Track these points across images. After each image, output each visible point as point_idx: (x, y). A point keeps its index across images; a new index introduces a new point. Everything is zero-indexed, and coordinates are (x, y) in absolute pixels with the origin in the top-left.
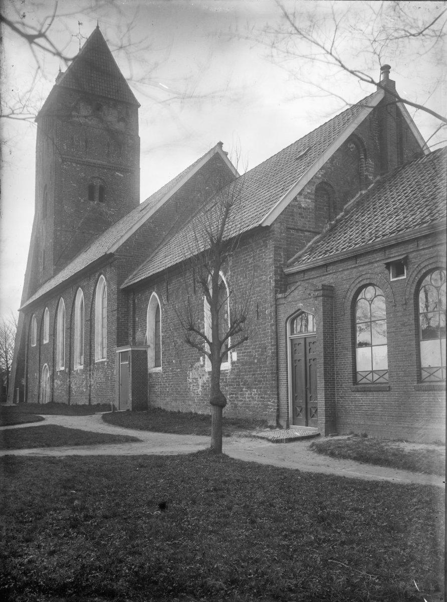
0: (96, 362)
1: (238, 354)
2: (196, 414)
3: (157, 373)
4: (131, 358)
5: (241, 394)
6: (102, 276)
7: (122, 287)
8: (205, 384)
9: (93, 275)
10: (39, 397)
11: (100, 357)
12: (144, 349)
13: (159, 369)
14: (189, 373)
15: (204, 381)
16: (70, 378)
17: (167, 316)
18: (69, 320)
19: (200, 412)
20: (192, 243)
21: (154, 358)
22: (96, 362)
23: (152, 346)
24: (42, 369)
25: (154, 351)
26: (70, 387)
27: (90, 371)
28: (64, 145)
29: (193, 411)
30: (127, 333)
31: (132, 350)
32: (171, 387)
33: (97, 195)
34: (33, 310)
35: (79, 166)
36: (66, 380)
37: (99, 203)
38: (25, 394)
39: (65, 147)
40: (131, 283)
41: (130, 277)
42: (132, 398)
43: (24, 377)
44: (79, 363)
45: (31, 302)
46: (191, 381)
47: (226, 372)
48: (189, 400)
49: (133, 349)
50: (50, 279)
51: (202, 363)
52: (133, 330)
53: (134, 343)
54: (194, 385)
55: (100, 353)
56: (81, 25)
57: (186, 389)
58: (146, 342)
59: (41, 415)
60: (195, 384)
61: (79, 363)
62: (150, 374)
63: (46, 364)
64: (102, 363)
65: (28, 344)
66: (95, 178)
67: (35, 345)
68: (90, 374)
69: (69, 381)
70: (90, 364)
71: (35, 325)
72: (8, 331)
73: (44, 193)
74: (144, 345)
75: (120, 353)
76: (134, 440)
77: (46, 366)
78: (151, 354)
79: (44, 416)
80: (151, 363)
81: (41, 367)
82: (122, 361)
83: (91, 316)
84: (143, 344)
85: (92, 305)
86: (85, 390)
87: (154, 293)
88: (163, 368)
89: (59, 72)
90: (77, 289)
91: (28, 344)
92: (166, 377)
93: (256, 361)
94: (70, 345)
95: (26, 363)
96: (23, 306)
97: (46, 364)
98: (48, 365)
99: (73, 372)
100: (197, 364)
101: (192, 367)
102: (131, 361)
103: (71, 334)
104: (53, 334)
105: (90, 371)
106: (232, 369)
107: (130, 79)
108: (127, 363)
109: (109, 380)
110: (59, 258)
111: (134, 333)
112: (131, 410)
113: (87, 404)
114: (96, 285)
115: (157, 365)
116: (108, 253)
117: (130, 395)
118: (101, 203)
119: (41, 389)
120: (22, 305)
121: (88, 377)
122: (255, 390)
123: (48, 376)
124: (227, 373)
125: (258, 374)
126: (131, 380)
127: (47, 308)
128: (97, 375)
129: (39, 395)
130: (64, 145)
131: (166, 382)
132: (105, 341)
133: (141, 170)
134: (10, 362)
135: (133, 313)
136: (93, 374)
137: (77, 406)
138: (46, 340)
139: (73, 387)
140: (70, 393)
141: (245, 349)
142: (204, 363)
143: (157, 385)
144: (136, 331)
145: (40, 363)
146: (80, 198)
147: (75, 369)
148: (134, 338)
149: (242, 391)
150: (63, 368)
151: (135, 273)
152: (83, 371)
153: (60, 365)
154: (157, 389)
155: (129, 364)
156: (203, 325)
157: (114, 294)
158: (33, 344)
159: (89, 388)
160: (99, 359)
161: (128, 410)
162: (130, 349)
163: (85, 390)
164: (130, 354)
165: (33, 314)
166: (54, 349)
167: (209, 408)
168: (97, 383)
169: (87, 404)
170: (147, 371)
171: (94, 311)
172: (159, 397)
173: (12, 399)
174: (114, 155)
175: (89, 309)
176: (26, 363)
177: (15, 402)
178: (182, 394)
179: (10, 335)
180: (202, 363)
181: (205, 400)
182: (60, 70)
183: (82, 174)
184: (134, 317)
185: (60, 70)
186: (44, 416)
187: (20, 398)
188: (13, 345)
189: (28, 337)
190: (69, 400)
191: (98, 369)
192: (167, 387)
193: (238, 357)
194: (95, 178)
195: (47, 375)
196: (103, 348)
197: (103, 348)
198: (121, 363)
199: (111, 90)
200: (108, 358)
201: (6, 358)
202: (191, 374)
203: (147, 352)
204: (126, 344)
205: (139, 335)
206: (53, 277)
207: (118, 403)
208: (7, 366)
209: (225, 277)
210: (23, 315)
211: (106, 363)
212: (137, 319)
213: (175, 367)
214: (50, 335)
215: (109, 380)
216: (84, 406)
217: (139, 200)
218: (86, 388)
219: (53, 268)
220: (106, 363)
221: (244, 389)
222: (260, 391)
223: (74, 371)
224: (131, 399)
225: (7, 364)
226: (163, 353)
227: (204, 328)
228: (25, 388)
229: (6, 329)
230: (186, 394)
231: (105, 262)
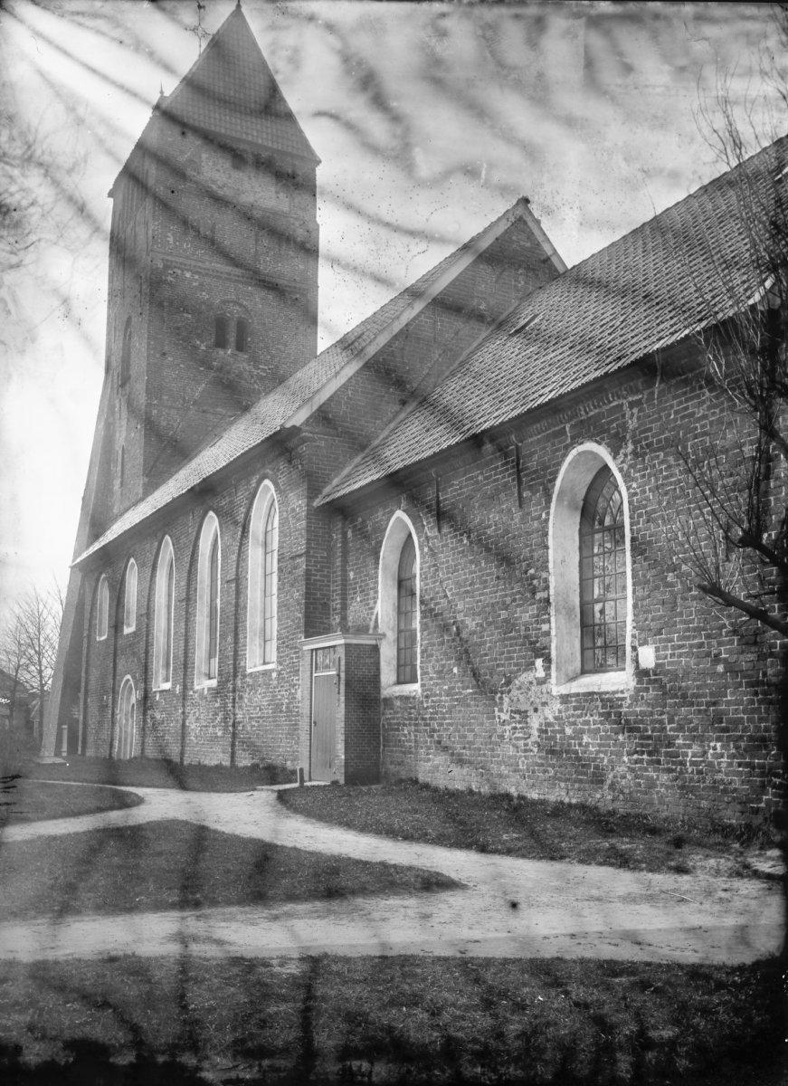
0: (249, 671)
1: (657, 650)
2: (521, 798)
3: (405, 699)
4: (343, 663)
5: (667, 754)
6: (267, 482)
7: (317, 503)
8: (548, 724)
9: (243, 482)
10: (111, 746)
11: (259, 660)
12: (374, 642)
13: (414, 689)
14: (501, 698)
15: (546, 719)
16: (184, 706)
17: (435, 565)
18: (183, 583)
19: (534, 795)
20: (393, 456)
21: (395, 662)
22: (249, 671)
23: (391, 636)
24: (119, 686)
25: (396, 647)
26: (184, 725)
27: (234, 691)
28: (169, 234)
29: (513, 791)
30: (326, 606)
31: (347, 646)
32: (447, 730)
33: (232, 338)
34: (104, 566)
35: (197, 277)
36: (176, 710)
37: (237, 353)
38: (80, 738)
39: (171, 240)
40: (338, 495)
41: (335, 482)
42: (345, 753)
43: (78, 704)
44: (205, 674)
45: (96, 549)
46: (504, 717)
47: (620, 695)
48: (499, 763)
49: (349, 641)
50: (135, 504)
51: (541, 673)
52: (342, 599)
53: (345, 630)
54: (515, 728)
55: (258, 651)
56: (202, 10)
57: (490, 737)
58: (376, 626)
59: (123, 788)
60: (518, 726)
61: (205, 674)
62: (386, 700)
63: (129, 677)
64: (266, 673)
65: (89, 636)
66: (229, 302)
67: (103, 638)
68: (234, 699)
69: (183, 713)
70: (235, 676)
71: (104, 594)
72: (45, 612)
73: (125, 333)
74: (371, 631)
75: (312, 650)
76: (433, 884)
77: (128, 680)
78: (388, 653)
79: (140, 791)
80: (387, 675)
81: (117, 688)
82: (316, 669)
83: (237, 571)
84: (368, 630)
85: (240, 547)
86: (220, 734)
87: (399, 514)
88: (423, 685)
89: (159, 95)
90: (206, 513)
91: (89, 636)
92: (433, 707)
93: (720, 668)
94: (186, 635)
95: (83, 675)
96: (78, 560)
97: (129, 677)
98: (134, 677)
99: (191, 693)
100: (525, 677)
101: (508, 682)
102: (343, 668)
103: (187, 612)
104: (147, 614)
105: (234, 691)
106: (637, 690)
107: (299, 113)
108: (334, 673)
109: (281, 711)
110: (155, 462)
111: (344, 607)
112: (342, 782)
113: (227, 763)
114: (251, 504)
115: (586, 668)
116: (288, 425)
117: (340, 747)
118: (240, 354)
119: (117, 729)
120: (75, 557)
121: (230, 705)
122: (719, 745)
123: (133, 700)
124: (623, 699)
125: (728, 703)
126: (343, 711)
127: (132, 560)
128: (250, 700)
129: (112, 740)
130: (169, 234)
131: (431, 719)
132: (274, 626)
133: (320, 290)
134: (48, 672)
135: (342, 561)
136: (241, 698)
137: (201, 768)
138: (129, 625)
139: (192, 725)
140: (183, 738)
141: (680, 639)
142: (548, 676)
143: (404, 725)
144: (349, 602)
145: (114, 676)
146: (198, 342)
147: (197, 687)
148: (344, 618)
149: (670, 745)
150: (167, 686)
151: (346, 472)
152: (217, 693)
153: (160, 679)
154: (405, 736)
155: (339, 675)
156: (546, 580)
157: (298, 520)
158: (100, 636)
159: (230, 728)
160: (255, 666)
161: (335, 783)
162: (342, 641)
163: (220, 734)
164: (341, 653)
165: (101, 573)
166: (148, 645)
167: (563, 785)
168: (250, 718)
169: (227, 763)
170: (379, 693)
171: (245, 560)
172: (411, 753)
173: (53, 749)
174: (268, 259)
175: (234, 557)
176: (83, 675)
177: (58, 754)
178: (480, 749)
179: (50, 619)
180: (541, 673)
181: (550, 765)
182: (162, 92)
183: (204, 293)
184: (345, 572)
185: (162, 92)
186: (140, 791)
187: (69, 743)
188: (55, 639)
189: (90, 621)
190: (182, 753)
191: (252, 687)
192: (434, 731)
193: (657, 658)
194: (229, 302)
195: (128, 699)
196: (265, 641)
197: (265, 641)
198: (315, 675)
199: (265, 130)
200: (280, 663)
201: (40, 665)
202: (506, 700)
203: (379, 649)
204: (326, 630)
205: (355, 610)
206: (142, 499)
207: (308, 765)
208: (41, 681)
209: (614, 458)
210: (79, 575)
211: (274, 675)
212: (352, 575)
213: (459, 684)
214: (139, 617)
215: (281, 711)
216: (219, 768)
217: (316, 348)
218: (225, 728)
219: (141, 481)
220: (274, 675)
221: (680, 741)
222: (737, 748)
223: (194, 692)
224: (343, 757)
225: (41, 677)
226: (422, 652)
227: (547, 588)
228: (81, 726)
229: (41, 607)
230: (493, 750)
231: (281, 445)
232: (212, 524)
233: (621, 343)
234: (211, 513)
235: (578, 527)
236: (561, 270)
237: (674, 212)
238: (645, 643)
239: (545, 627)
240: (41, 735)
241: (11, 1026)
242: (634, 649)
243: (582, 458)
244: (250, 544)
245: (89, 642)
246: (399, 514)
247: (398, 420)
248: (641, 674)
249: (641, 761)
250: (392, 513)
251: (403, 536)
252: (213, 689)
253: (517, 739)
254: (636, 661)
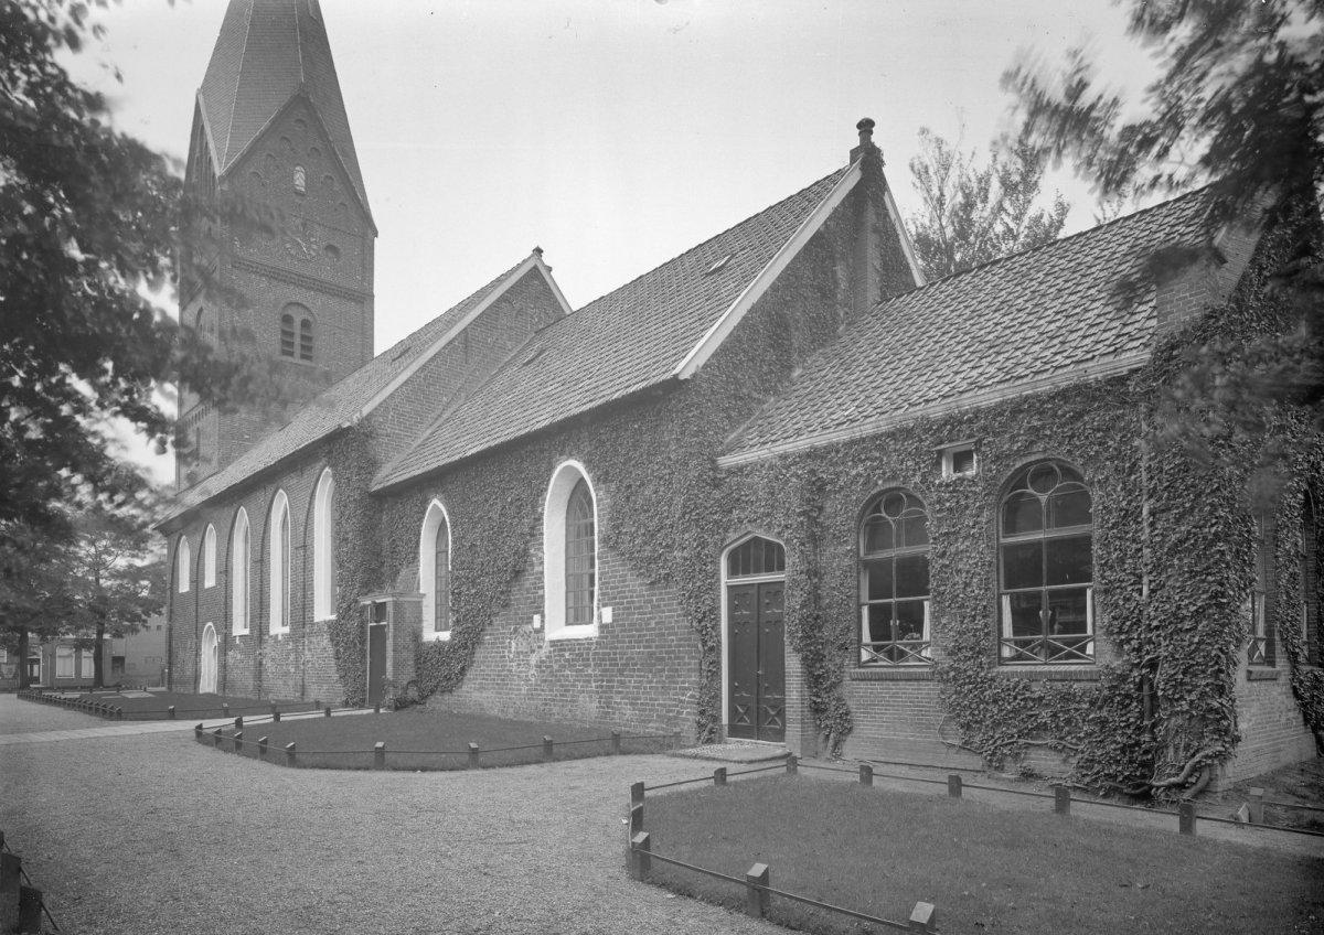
8: (542, 662)
14: (510, 643)
63: (210, 624)
83: (305, 538)
87: (435, 501)
104: (225, 571)
106: (600, 637)
163: (293, 670)
232: (281, 502)
233: (645, 367)
234: (281, 491)
235: (564, 515)
236: (568, 312)
237: (832, 223)
238: (605, 605)
239: (540, 592)
240: (674, 756)
241: (7, 828)
242: (599, 608)
243: (572, 465)
244: (547, 503)
245: (172, 593)
246: (435, 501)
247: (436, 425)
248: (603, 627)
249: (602, 687)
250: (425, 502)
251: (439, 519)
252: (286, 635)
253: (520, 672)
254: (600, 617)
